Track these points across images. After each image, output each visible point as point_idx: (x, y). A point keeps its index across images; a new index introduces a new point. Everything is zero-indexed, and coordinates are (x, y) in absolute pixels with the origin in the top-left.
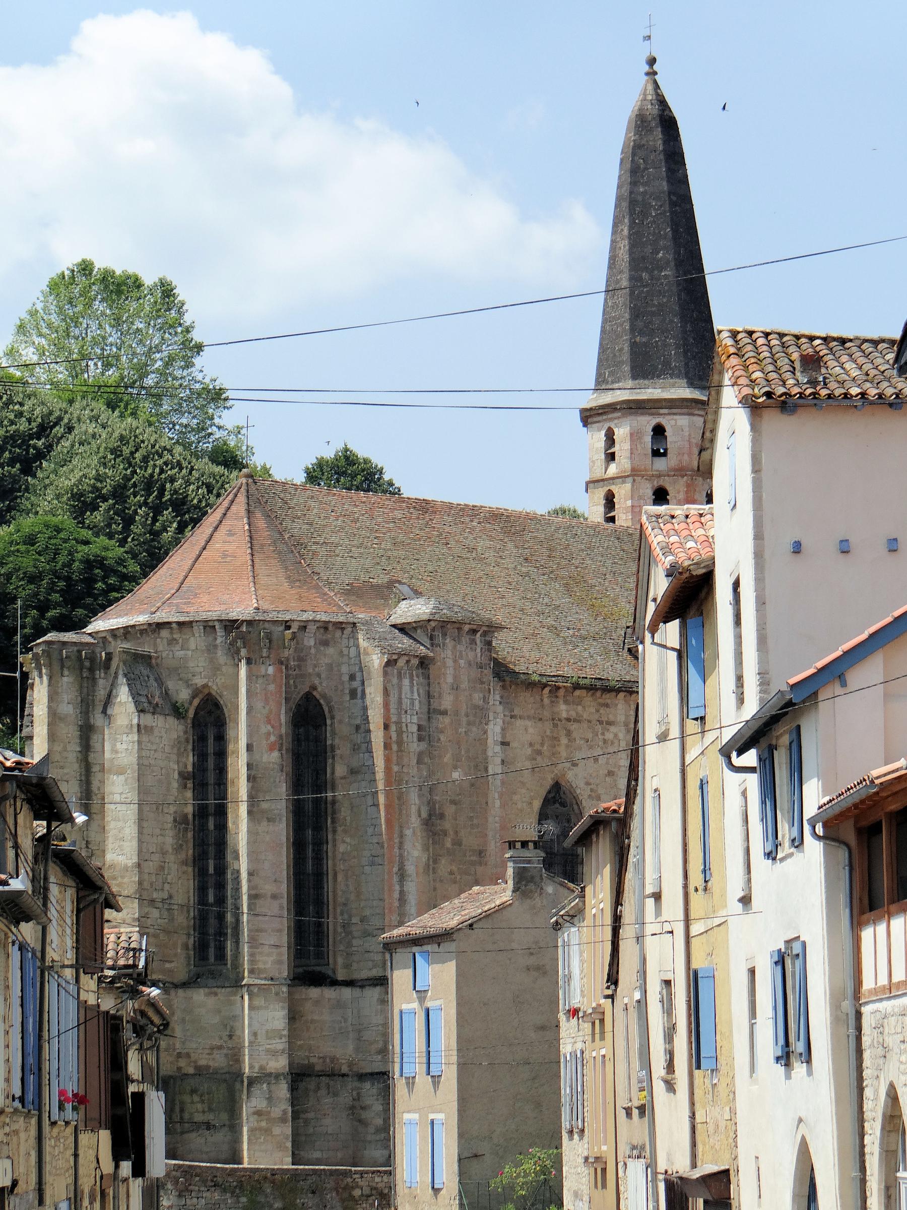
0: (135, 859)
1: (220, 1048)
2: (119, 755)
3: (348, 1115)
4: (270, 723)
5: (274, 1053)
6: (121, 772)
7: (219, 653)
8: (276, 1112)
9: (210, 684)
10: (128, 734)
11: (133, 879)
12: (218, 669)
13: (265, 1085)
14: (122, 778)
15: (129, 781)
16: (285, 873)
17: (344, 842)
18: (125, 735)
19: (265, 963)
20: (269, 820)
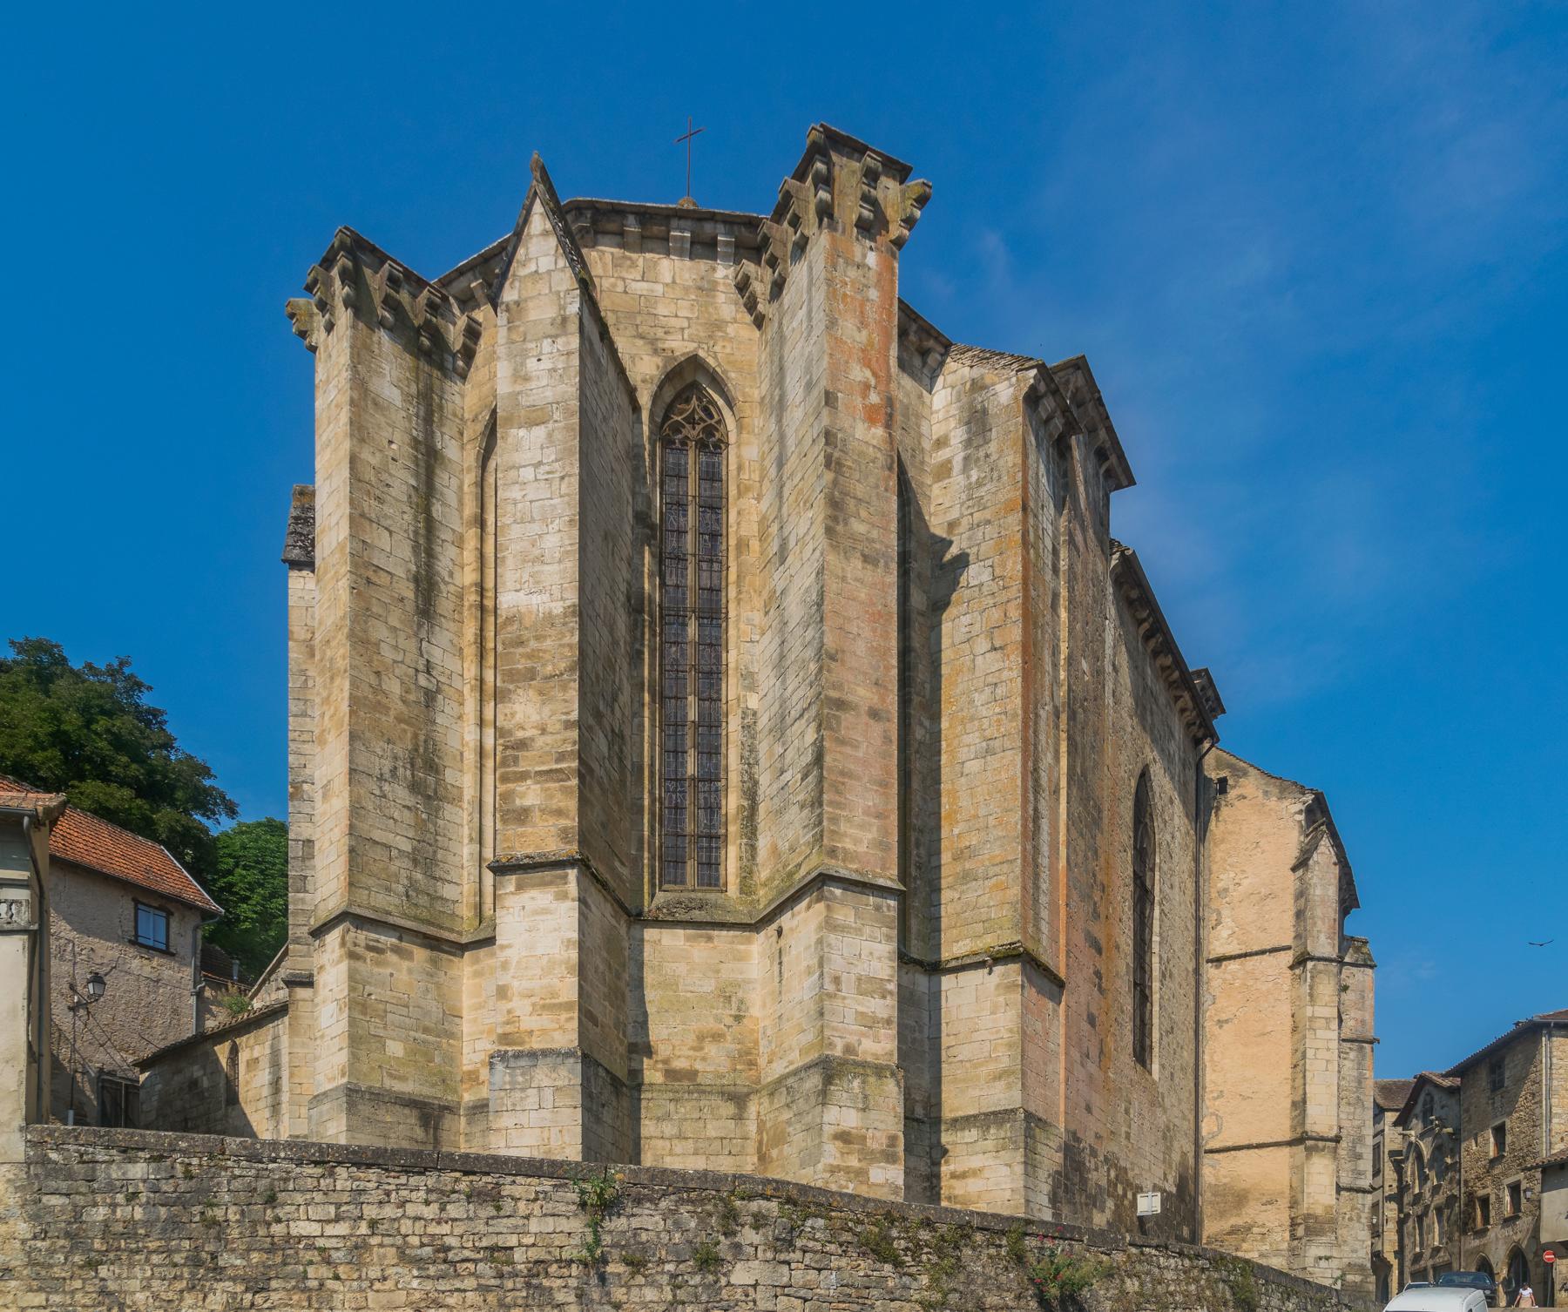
0: (572, 598)
1: (717, 1037)
2: (533, 385)
3: (925, 1189)
4: (869, 366)
5: (869, 1022)
6: (536, 418)
7: (721, 298)
8: (877, 1142)
9: (702, 354)
10: (554, 338)
11: (566, 640)
12: (719, 328)
13: (856, 1083)
14: (539, 433)
15: (558, 436)
16: (895, 672)
17: (921, 724)
18: (547, 343)
19: (856, 841)
20: (866, 559)
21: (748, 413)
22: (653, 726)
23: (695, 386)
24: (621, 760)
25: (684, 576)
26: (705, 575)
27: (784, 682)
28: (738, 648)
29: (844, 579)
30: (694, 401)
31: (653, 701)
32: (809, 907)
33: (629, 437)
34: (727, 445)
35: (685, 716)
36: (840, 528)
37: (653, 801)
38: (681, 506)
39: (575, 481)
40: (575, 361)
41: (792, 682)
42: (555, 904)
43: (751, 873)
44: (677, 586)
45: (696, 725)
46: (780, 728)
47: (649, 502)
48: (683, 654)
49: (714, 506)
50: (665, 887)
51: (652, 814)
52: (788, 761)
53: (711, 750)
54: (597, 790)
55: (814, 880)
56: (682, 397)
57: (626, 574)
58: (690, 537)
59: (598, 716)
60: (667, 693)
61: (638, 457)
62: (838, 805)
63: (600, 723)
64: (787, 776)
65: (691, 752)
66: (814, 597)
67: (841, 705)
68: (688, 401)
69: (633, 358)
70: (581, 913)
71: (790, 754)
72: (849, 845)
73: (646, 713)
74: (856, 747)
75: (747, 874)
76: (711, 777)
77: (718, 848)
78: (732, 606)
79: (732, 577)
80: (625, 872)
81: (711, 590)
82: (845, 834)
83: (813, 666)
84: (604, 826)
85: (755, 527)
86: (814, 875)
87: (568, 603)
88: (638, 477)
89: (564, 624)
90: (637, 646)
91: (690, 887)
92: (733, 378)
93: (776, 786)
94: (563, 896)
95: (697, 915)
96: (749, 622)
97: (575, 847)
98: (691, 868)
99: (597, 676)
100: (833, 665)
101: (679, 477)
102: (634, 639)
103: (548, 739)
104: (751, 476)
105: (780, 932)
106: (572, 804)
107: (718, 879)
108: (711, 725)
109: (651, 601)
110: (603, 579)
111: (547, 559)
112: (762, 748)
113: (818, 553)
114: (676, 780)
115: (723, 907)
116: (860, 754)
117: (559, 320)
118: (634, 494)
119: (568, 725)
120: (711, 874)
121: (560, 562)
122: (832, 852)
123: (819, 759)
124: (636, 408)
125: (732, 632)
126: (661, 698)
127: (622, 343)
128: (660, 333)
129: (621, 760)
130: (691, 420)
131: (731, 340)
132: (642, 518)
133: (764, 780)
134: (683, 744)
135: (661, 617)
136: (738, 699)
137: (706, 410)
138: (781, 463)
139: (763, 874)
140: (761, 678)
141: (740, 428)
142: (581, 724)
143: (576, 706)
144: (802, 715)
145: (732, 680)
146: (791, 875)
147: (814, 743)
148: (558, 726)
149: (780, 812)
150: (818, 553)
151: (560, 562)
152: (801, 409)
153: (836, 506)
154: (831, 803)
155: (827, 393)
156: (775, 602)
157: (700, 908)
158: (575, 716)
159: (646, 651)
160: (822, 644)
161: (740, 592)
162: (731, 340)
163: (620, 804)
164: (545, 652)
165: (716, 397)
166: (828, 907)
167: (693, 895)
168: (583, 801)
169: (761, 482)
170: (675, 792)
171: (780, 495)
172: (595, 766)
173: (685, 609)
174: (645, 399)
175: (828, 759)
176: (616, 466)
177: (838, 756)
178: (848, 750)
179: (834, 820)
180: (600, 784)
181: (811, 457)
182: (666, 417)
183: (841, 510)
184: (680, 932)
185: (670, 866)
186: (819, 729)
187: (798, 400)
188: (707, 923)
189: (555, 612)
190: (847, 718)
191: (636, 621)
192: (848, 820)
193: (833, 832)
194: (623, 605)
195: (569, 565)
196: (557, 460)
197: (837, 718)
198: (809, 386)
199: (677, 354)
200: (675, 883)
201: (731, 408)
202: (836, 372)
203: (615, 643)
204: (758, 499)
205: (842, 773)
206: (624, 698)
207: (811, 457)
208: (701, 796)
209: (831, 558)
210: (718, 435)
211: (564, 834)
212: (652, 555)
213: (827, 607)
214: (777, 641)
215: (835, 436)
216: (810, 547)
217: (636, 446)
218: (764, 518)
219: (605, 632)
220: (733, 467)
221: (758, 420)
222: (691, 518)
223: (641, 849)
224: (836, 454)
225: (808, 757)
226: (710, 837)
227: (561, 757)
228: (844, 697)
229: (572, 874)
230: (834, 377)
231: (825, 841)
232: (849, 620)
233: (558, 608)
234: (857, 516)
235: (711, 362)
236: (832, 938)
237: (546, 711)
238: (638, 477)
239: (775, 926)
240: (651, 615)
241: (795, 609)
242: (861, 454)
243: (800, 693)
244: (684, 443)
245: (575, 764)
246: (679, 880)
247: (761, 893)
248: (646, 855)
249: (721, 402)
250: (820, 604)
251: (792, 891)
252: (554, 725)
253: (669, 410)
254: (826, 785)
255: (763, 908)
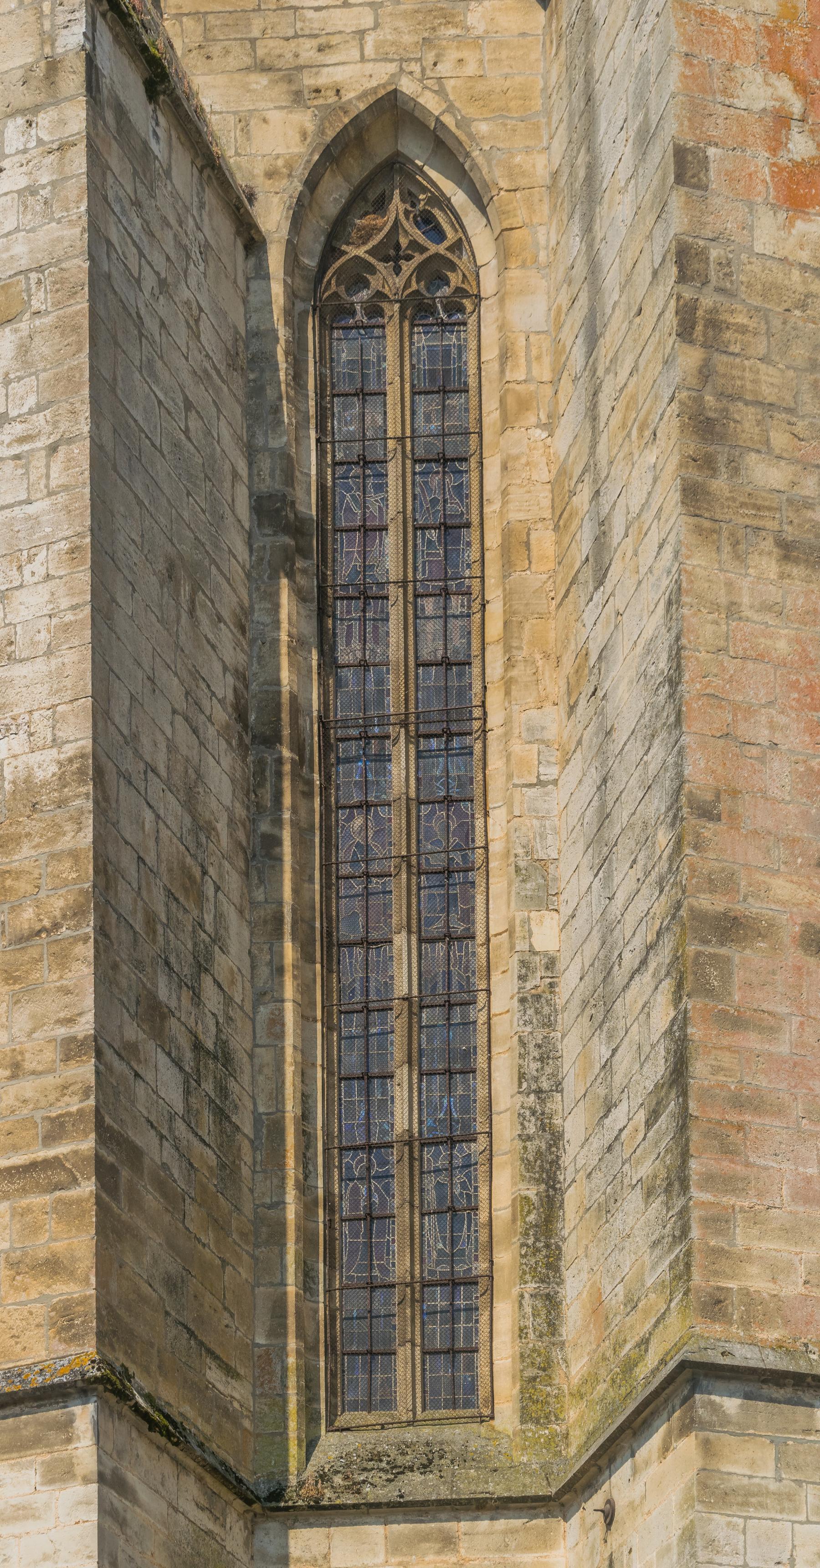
0: (78, 737)
9: (407, 86)
10: (29, 114)
11: (66, 843)
19: (777, 1270)
21: (521, 216)
22: (305, 1018)
23: (395, 167)
24: (221, 1115)
25: (381, 638)
26: (431, 628)
27: (609, 877)
28: (509, 804)
29: (732, 610)
30: (397, 205)
31: (306, 956)
32: (666, 1449)
33: (237, 316)
34: (478, 298)
35: (388, 986)
36: (720, 484)
37: (308, 1209)
38: (369, 464)
39: (81, 451)
40: (78, 161)
41: (625, 880)
42: (45, 1494)
43: (547, 1367)
44: (364, 665)
45: (415, 1006)
46: (602, 1004)
47: (289, 469)
48: (382, 831)
49: (449, 459)
50: (345, 1418)
51: (307, 1239)
52: (618, 1080)
53: (454, 1066)
54: (152, 1200)
55: (669, 1380)
56: (367, 197)
57: (232, 655)
58: (391, 540)
59: (154, 1014)
60: (345, 933)
61: (262, 361)
62: (727, 1183)
63: (158, 1034)
64: (619, 1115)
65: (402, 1074)
66: (663, 665)
67: (730, 928)
68: (381, 205)
69: (244, 122)
70: (106, 1511)
71: (624, 1061)
72: (757, 1282)
73: (289, 990)
74: (770, 1031)
75: (538, 1370)
76: (453, 1134)
77: (471, 1310)
78: (494, 699)
79: (494, 629)
80: (238, 1392)
81: (446, 663)
82: (747, 1257)
83: (664, 838)
84: (173, 1285)
85: (544, 497)
86: (672, 1365)
87: (70, 750)
88: (259, 410)
89: (61, 804)
90: (265, 827)
91: (405, 1421)
92: (484, 136)
93: (597, 1143)
94: (60, 1474)
95: (417, 1486)
96: (534, 736)
97: (90, 1348)
98: (405, 1365)
99: (151, 920)
100: (709, 830)
101: (363, 394)
102: (257, 810)
103: (27, 1087)
104: (531, 371)
105: (609, 1515)
106: (80, 1244)
107: (472, 1388)
108: (451, 999)
109: (296, 709)
110: (165, 677)
111: (21, 649)
112: (570, 1047)
113: (668, 551)
114: (369, 1148)
115: (479, 1460)
116: (784, 1049)
117: (41, 70)
118: (251, 453)
119: (71, 1049)
120: (455, 1382)
121: (49, 652)
122: (715, 1305)
123: (679, 1073)
124: (253, 243)
125: (495, 763)
126: (327, 945)
127: (213, 91)
128: (307, 51)
129: (221, 1115)
130: (391, 253)
131: (477, 42)
132: (271, 510)
133: (573, 1128)
134: (384, 1059)
135: (326, 746)
136: (511, 931)
137: (427, 221)
138: (592, 337)
139: (575, 1366)
140: (564, 870)
141: (505, 255)
142: (101, 1046)
143: (89, 1001)
144: (644, 962)
145: (498, 885)
146: (629, 1366)
147: (669, 1032)
148: (50, 1054)
149: (605, 1209)
150: (668, 551)
151: (49, 652)
152: (628, 198)
153: (708, 431)
154: (709, 1180)
155: (681, 154)
156: (586, 680)
157: (425, 1468)
158: (86, 1026)
159: (287, 836)
160: (680, 780)
161: (510, 664)
162: (477, 42)
163: (220, 1226)
164: (17, 875)
165: (447, 186)
166: (707, 1447)
167: (409, 1434)
168: (111, 1231)
169: (555, 382)
170: (366, 1178)
171: (592, 413)
172: (146, 1140)
173: (384, 721)
174: (272, 217)
175: (700, 1070)
176: (198, 394)
177: (727, 1060)
178: (752, 1041)
179: (719, 1222)
180: (162, 1186)
181: (650, 314)
182: (330, 252)
183: (723, 438)
184: (376, 1532)
185: (352, 1364)
186: (677, 999)
187: (623, 174)
188: (442, 1504)
189: (40, 775)
190: (746, 959)
191: (261, 764)
192: (754, 1218)
193: (718, 1253)
194: (224, 732)
195: (70, 657)
196: (39, 408)
197: (723, 964)
198: (644, 139)
199: (349, 95)
200: (369, 1407)
201: (482, 209)
202: (698, 100)
203: (202, 828)
204: (550, 427)
205: (738, 1102)
206: (231, 961)
207: (650, 314)
208: (430, 1182)
209: (700, 561)
210: (455, 279)
211: (64, 1320)
212: (300, 595)
213: (690, 688)
214: (594, 777)
215: (702, 255)
216: (654, 538)
217: (255, 334)
218: (563, 472)
219: (172, 807)
220: (490, 353)
221: (546, 232)
222: (394, 497)
223: (278, 1330)
224: (707, 301)
225: (658, 1069)
226: (453, 1283)
227: (56, 1130)
228: (739, 908)
229: (84, 1415)
230: (696, 112)
231: (697, 1278)
232: (749, 711)
233: (45, 765)
234: (765, 447)
235: (431, 103)
236: (719, 1524)
237: (22, 1020)
238: (259, 410)
239: (598, 1500)
240: (299, 747)
241: (628, 697)
242: (769, 290)
243: (640, 905)
244: (374, 310)
245: (87, 1144)
246: (378, 1399)
247: (572, 1415)
248: (292, 1344)
249: (459, 198)
250: (673, 682)
251: (631, 1407)
252: (41, 1053)
253: (337, 232)
254: (695, 1136)
255: (576, 1452)
